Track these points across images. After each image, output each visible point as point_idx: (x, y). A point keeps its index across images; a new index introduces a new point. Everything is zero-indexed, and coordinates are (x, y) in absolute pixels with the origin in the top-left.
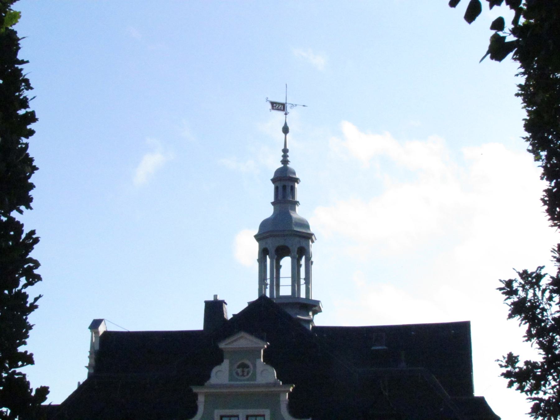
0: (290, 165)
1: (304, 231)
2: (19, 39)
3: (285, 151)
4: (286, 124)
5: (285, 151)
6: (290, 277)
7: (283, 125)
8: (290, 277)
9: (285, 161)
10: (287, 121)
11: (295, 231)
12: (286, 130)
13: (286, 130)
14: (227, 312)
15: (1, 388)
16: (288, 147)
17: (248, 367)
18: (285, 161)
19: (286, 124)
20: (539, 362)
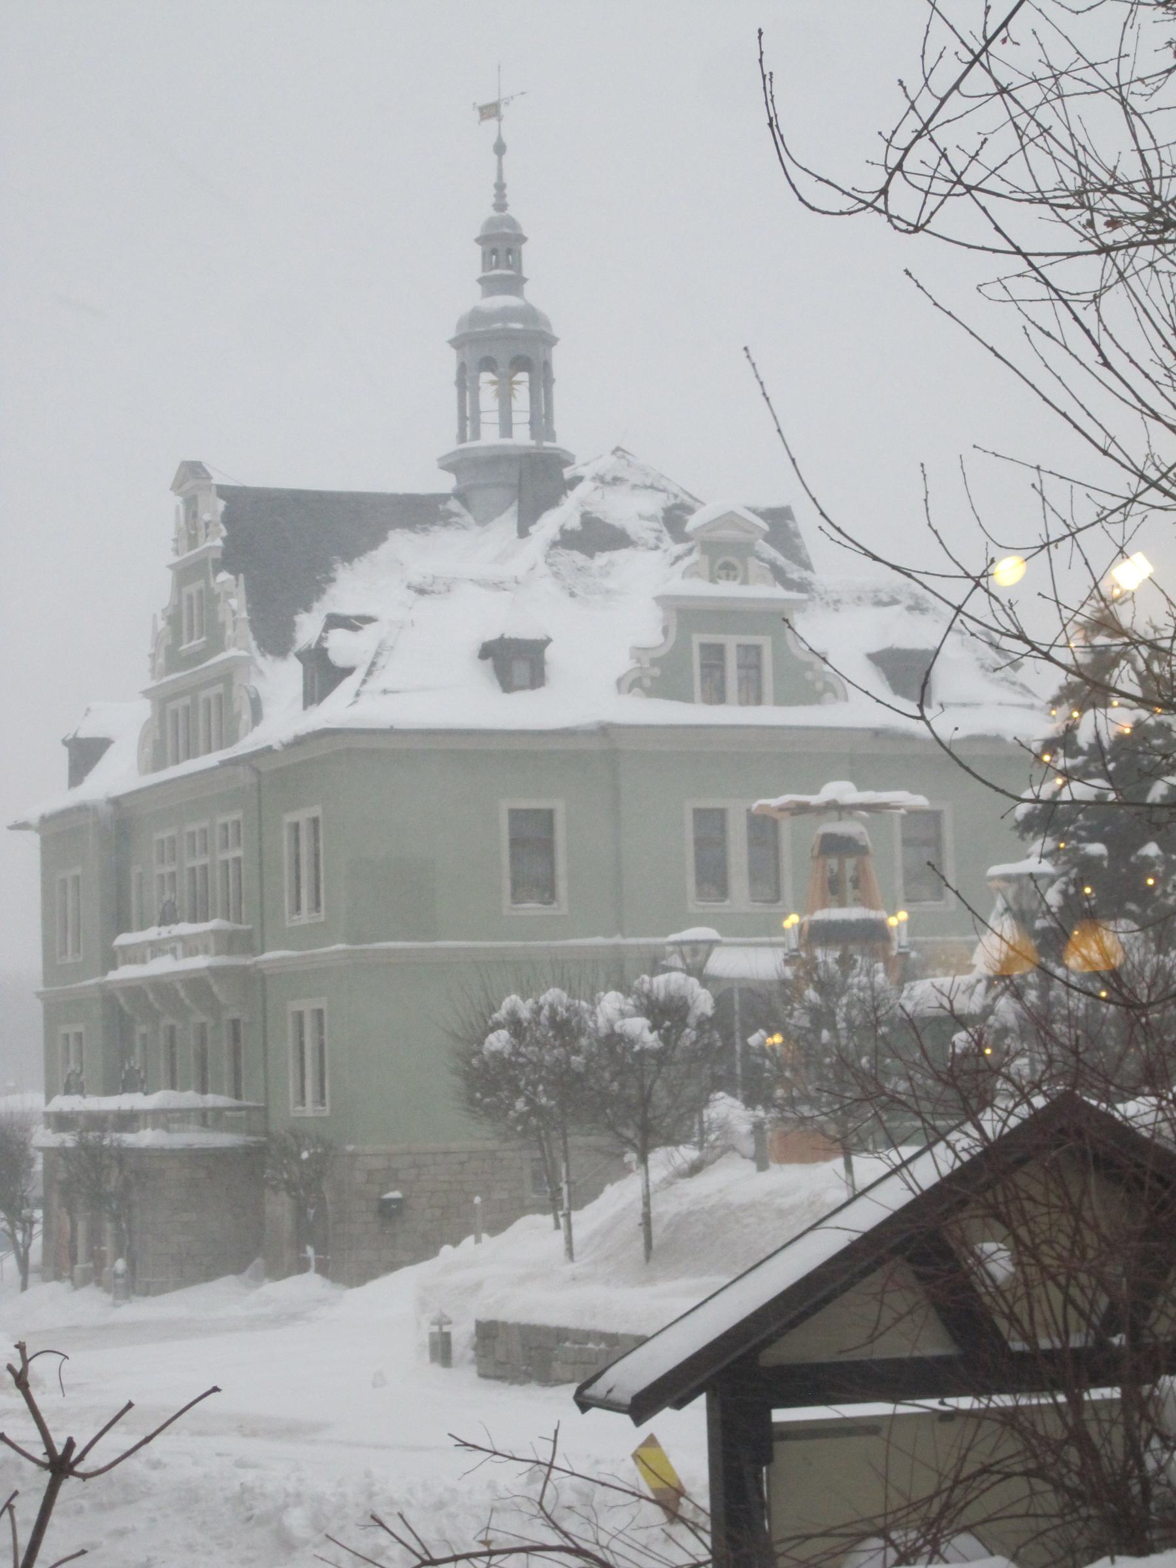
0: (511, 211)
1: (921, 1269)
2: (896, 1149)
3: (500, 187)
4: (500, 138)
5: (500, 187)
6: (938, 98)
7: (494, 139)
8: (938, 98)
9: (500, 206)
10: (502, 134)
11: (993, 1322)
12: (500, 148)
13: (500, 148)
14: (149, 1297)
15: (1174, 857)
16: (496, 157)
17: (734, 568)
18: (500, 206)
19: (500, 138)
20: (630, 684)
